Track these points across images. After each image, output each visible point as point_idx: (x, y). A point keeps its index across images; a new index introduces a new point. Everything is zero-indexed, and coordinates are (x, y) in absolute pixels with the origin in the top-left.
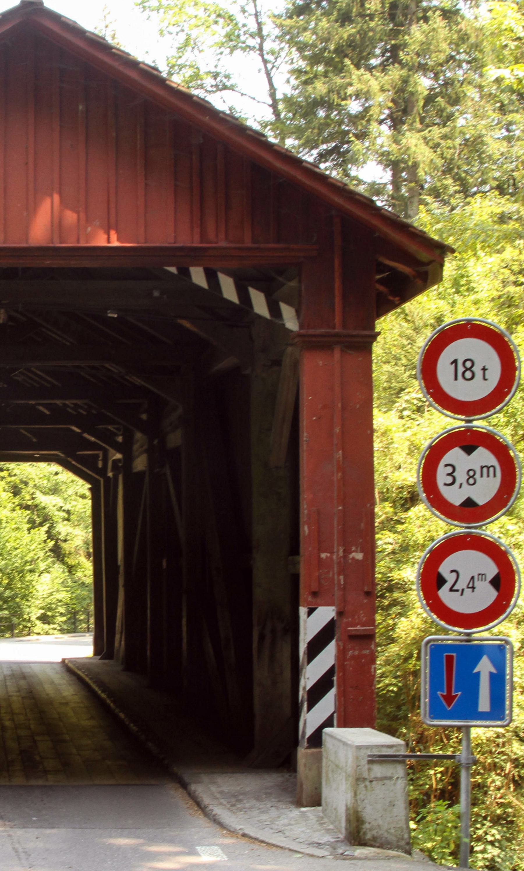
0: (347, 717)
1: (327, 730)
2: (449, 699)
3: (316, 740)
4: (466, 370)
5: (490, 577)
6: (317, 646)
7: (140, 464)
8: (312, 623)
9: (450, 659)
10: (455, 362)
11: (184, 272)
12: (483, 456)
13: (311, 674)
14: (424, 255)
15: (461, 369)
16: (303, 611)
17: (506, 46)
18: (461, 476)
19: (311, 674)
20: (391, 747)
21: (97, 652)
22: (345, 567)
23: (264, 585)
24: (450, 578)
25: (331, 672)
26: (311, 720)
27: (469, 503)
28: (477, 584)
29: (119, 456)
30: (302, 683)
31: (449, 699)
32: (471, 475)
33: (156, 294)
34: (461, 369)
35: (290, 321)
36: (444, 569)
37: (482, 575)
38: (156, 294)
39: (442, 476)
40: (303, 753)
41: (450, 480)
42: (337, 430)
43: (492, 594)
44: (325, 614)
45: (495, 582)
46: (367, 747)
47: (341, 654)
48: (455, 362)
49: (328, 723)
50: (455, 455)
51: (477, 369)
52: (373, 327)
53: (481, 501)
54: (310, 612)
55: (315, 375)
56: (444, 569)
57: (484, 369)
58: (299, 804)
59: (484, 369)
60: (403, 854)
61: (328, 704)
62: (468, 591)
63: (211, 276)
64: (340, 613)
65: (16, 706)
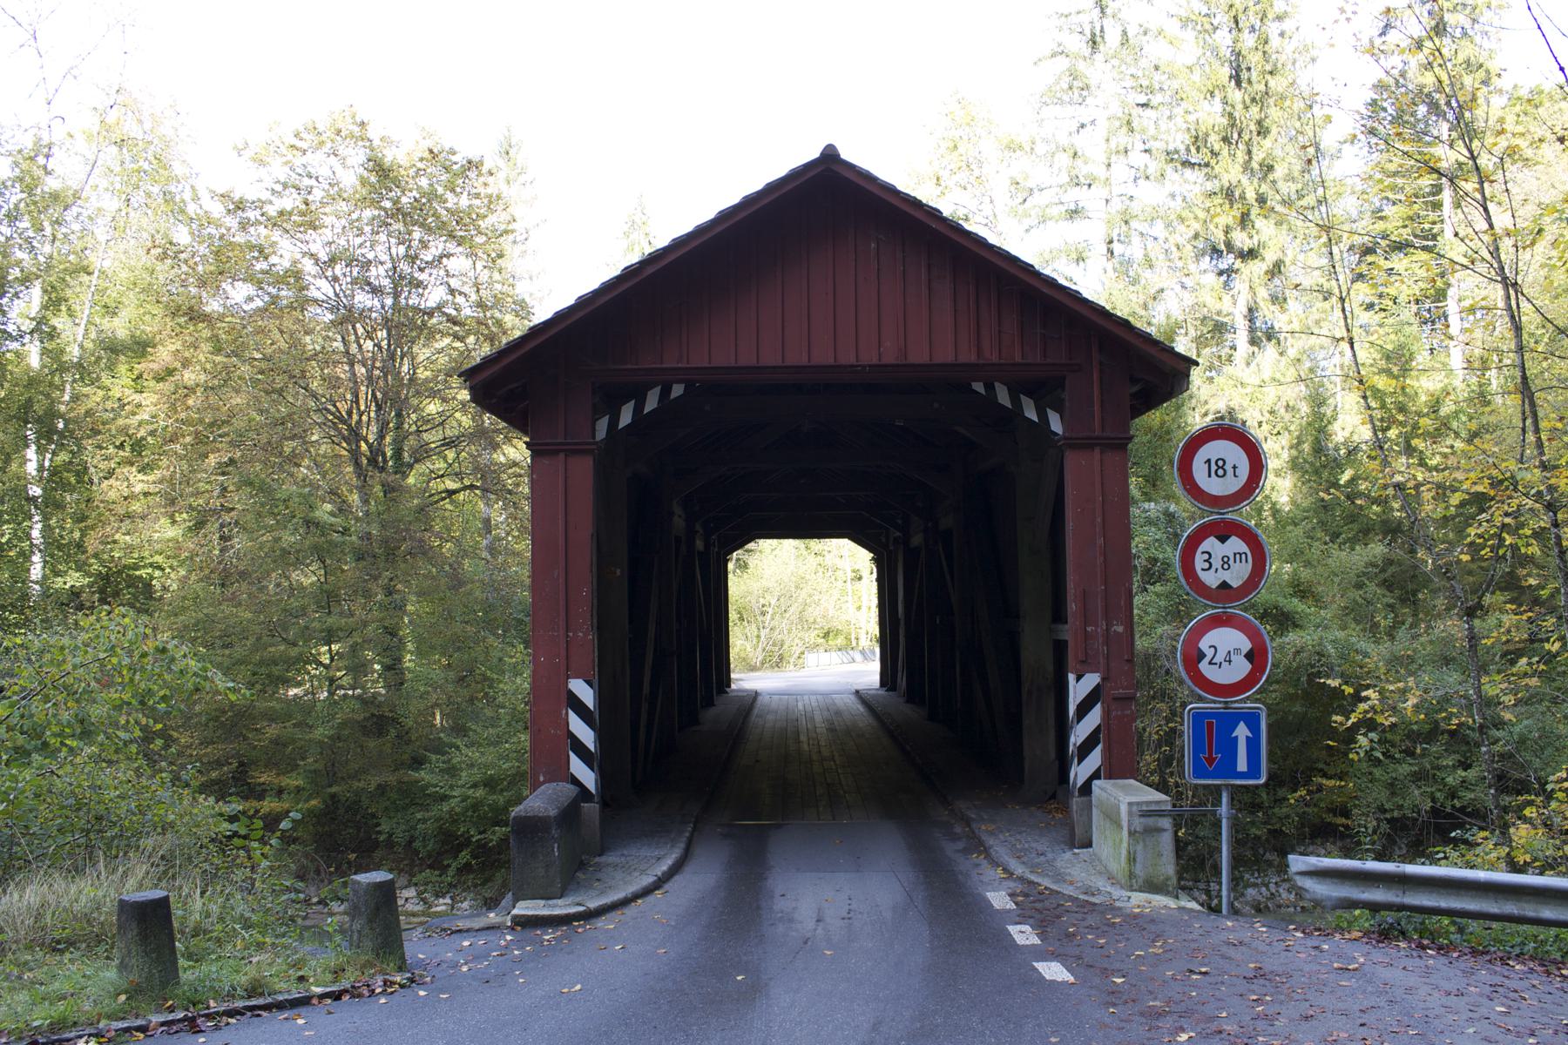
0: (1111, 770)
1: (1096, 782)
2: (1210, 760)
3: (1086, 789)
4: (1218, 468)
5: (1244, 651)
6: (1084, 708)
7: (917, 540)
8: (1078, 689)
9: (1210, 725)
10: (1209, 461)
12: (1236, 544)
13: (1080, 733)
15: (1214, 467)
16: (1071, 677)
17: (140, 347)
18: (1217, 563)
19: (1080, 733)
20: (1158, 803)
21: (883, 683)
22: (1108, 638)
23: (1034, 651)
24: (1209, 653)
25: (1097, 730)
26: (1080, 772)
27: (1224, 585)
30: (1072, 740)
31: (1210, 760)
32: (1225, 562)
33: (936, 405)
34: (1214, 467)
35: (1056, 425)
37: (1237, 650)
38: (936, 405)
39: (1199, 562)
40: (1076, 802)
41: (1206, 565)
42: (1099, 520)
43: (1247, 667)
44: (1091, 680)
45: (1249, 656)
47: (1106, 714)
48: (1209, 461)
49: (1096, 775)
50: (1211, 544)
51: (1228, 467)
53: (1235, 584)
54: (1078, 678)
55: (1079, 469)
56: (1204, 644)
57: (1235, 467)
58: (1072, 846)
59: (1235, 467)
61: (1095, 759)
63: (990, 387)
64: (1103, 679)
65: (818, 718)
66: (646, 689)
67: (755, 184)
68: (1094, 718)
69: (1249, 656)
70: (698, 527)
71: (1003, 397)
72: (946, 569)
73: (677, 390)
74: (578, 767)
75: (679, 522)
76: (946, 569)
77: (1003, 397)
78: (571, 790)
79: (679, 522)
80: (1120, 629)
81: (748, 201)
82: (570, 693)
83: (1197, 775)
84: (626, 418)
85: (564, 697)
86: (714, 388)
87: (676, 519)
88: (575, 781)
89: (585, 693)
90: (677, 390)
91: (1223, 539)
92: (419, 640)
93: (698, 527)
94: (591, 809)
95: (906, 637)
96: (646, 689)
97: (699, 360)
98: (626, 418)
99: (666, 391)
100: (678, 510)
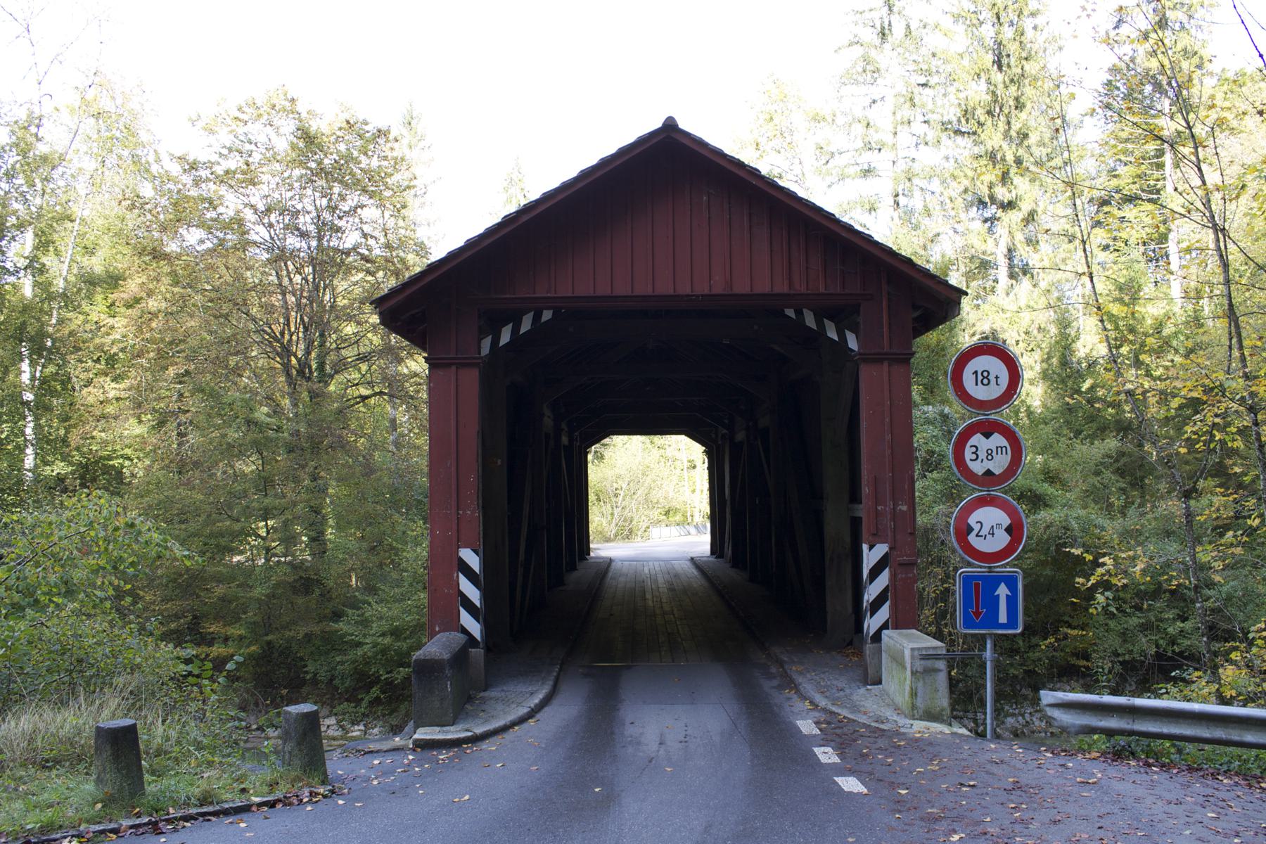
0: (897, 622)
1: (885, 632)
2: (977, 614)
3: (877, 637)
4: (984, 378)
5: (1005, 526)
6: (875, 572)
7: (740, 436)
8: (871, 557)
9: (977, 585)
10: (976, 372)
11: (799, 313)
12: (998, 440)
13: (872, 592)
14: (954, 295)
15: (980, 378)
16: (865, 547)
17: (113, 280)
18: (982, 454)
19: (872, 592)
21: (713, 552)
22: (894, 515)
23: (835, 525)
24: (976, 527)
25: (886, 590)
26: (872, 624)
27: (989, 473)
28: (996, 531)
29: (725, 431)
30: (866, 597)
31: (977, 614)
32: (989, 453)
33: (756, 327)
34: (980, 378)
35: (853, 343)
36: (972, 520)
37: (999, 525)
38: (756, 327)
39: (968, 454)
40: (869, 648)
41: (974, 457)
42: (887, 420)
43: (1007, 538)
44: (881, 549)
45: (1009, 530)
46: (919, 649)
47: (893, 577)
48: (976, 372)
49: (885, 626)
50: (977, 439)
51: (992, 377)
52: (910, 346)
53: (997, 472)
54: (871, 548)
55: (871, 379)
56: (972, 520)
57: (997, 377)
59: (997, 377)
60: (908, 688)
61: (884, 613)
62: (989, 537)
63: (799, 313)
64: (891, 548)
66: (522, 556)
68: (883, 580)
69: (1009, 530)
70: (564, 426)
73: (547, 315)
74: (466, 620)
75: (548, 421)
78: (461, 638)
79: (548, 421)
80: (904, 508)
82: (461, 560)
84: (505, 337)
85: (455, 563)
86: (576, 313)
87: (546, 419)
88: (464, 631)
90: (547, 315)
91: (987, 435)
92: (339, 517)
93: (564, 426)
94: (477, 654)
96: (522, 556)
97: (565, 291)
98: (505, 337)
99: (538, 316)
100: (547, 412)
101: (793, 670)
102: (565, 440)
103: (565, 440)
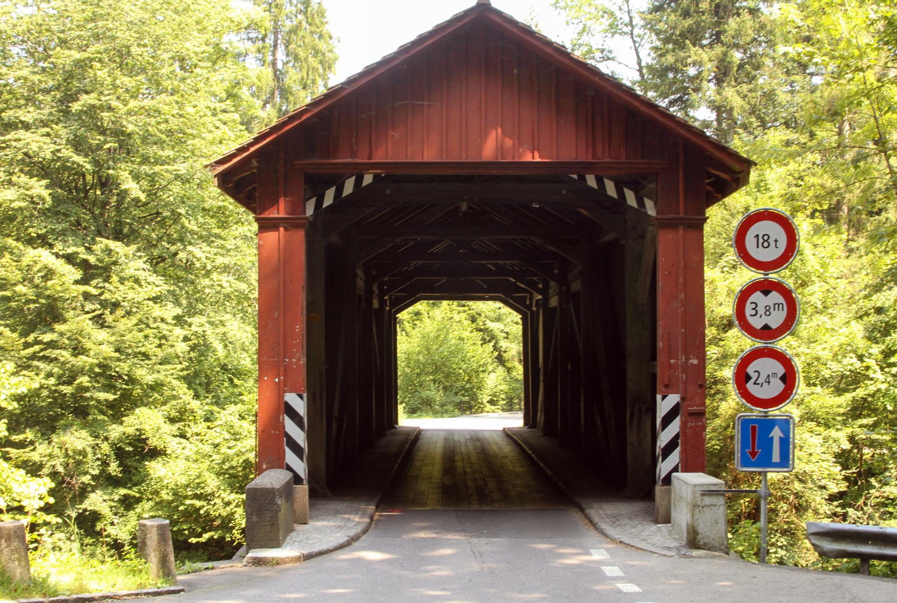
0: (687, 466)
1: (674, 474)
2: (753, 454)
3: (667, 480)
4: (764, 241)
5: (780, 375)
6: (668, 419)
7: (554, 302)
8: (664, 405)
9: (754, 428)
10: (757, 236)
12: (775, 297)
13: (664, 438)
14: (737, 167)
15: (761, 241)
16: (659, 397)
18: (761, 310)
19: (664, 438)
20: (716, 485)
21: (526, 424)
23: (634, 381)
24: (754, 376)
25: (677, 437)
26: (664, 467)
27: (766, 327)
29: (540, 297)
30: (658, 444)
31: (753, 454)
32: (767, 310)
33: (564, 192)
34: (761, 241)
35: (651, 209)
36: (750, 370)
38: (564, 192)
39: (748, 310)
40: (659, 489)
41: (754, 312)
42: (681, 280)
43: (782, 386)
44: (673, 399)
45: (783, 379)
46: (701, 485)
47: (684, 425)
48: (757, 236)
49: (675, 469)
50: (757, 296)
51: (771, 241)
52: (704, 214)
53: (774, 326)
54: (664, 398)
55: (667, 244)
56: (750, 370)
57: (776, 241)
58: (656, 522)
59: (776, 241)
61: (675, 458)
62: (765, 385)
63: (599, 180)
64: (683, 399)
66: (336, 413)
67: (428, 26)
68: (674, 427)
69: (783, 379)
70: (375, 289)
71: (611, 189)
72: (574, 319)
73: (368, 179)
74: (290, 457)
75: (361, 283)
76: (574, 319)
77: (611, 189)
78: (289, 475)
79: (361, 283)
80: (695, 362)
81: (422, 39)
82: (287, 404)
83: (744, 464)
84: (328, 200)
85: (283, 406)
86: (396, 177)
87: (358, 280)
88: (289, 468)
89: (300, 406)
90: (368, 179)
91: (766, 293)
92: (128, 390)
93: (375, 289)
94: (302, 491)
95: (544, 381)
96: (336, 413)
97: (379, 157)
98: (328, 200)
99: (359, 179)
100: (360, 273)
101: (591, 512)
102: (376, 304)
103: (376, 304)
